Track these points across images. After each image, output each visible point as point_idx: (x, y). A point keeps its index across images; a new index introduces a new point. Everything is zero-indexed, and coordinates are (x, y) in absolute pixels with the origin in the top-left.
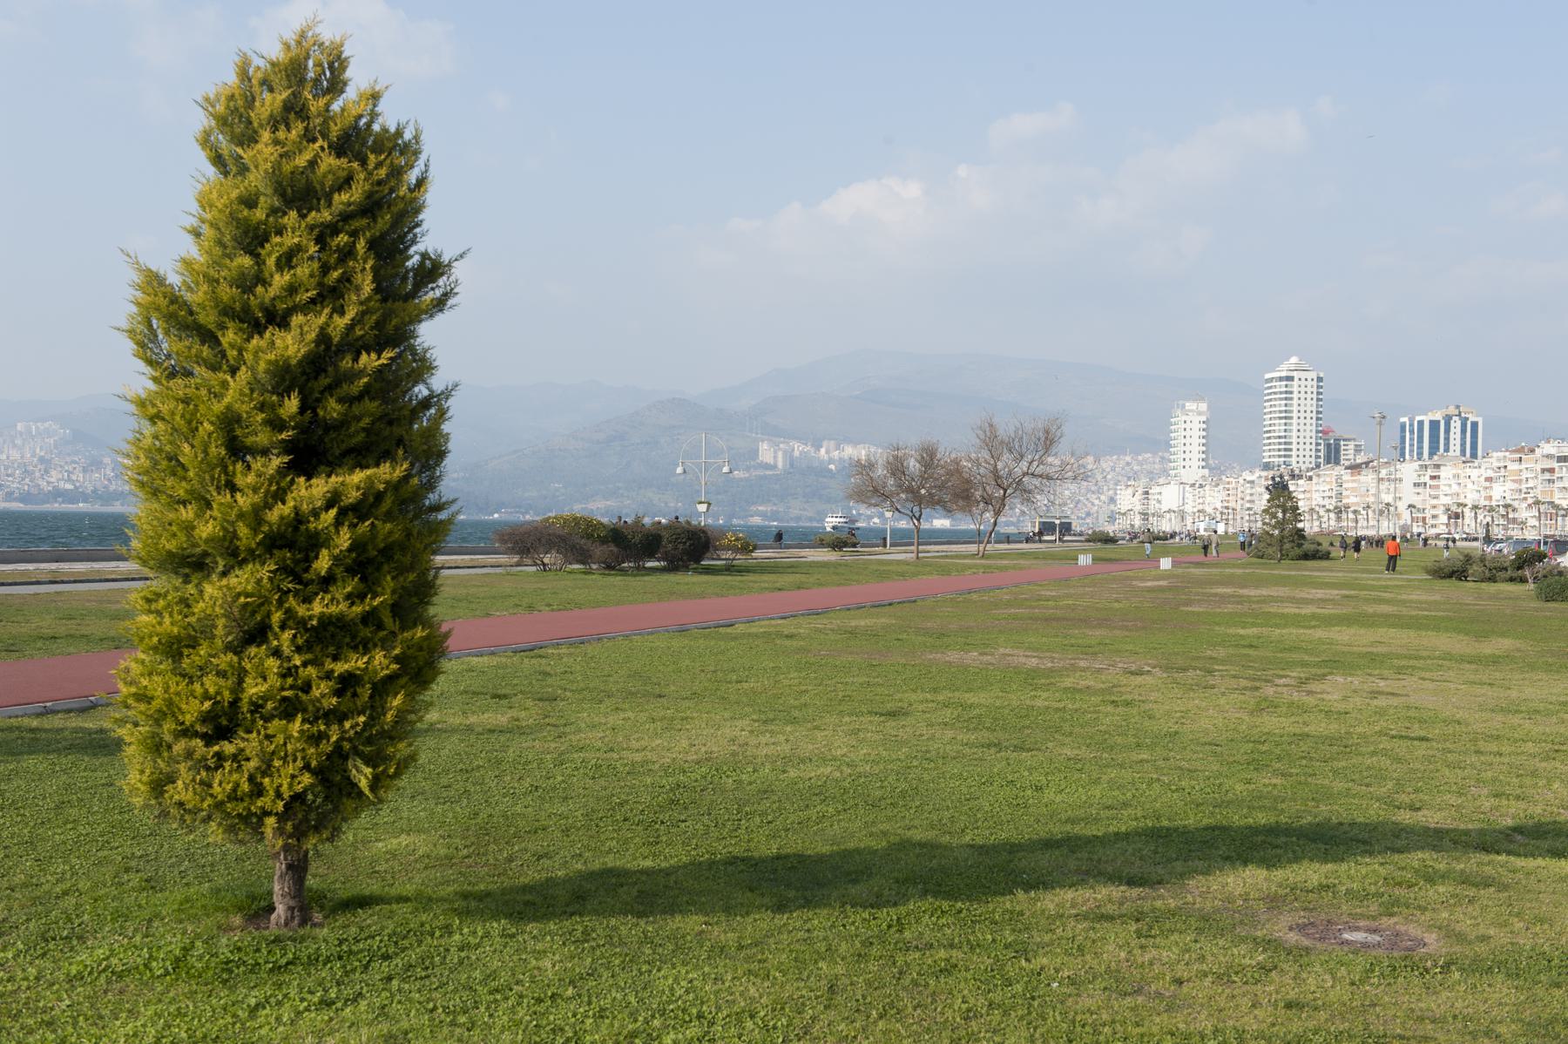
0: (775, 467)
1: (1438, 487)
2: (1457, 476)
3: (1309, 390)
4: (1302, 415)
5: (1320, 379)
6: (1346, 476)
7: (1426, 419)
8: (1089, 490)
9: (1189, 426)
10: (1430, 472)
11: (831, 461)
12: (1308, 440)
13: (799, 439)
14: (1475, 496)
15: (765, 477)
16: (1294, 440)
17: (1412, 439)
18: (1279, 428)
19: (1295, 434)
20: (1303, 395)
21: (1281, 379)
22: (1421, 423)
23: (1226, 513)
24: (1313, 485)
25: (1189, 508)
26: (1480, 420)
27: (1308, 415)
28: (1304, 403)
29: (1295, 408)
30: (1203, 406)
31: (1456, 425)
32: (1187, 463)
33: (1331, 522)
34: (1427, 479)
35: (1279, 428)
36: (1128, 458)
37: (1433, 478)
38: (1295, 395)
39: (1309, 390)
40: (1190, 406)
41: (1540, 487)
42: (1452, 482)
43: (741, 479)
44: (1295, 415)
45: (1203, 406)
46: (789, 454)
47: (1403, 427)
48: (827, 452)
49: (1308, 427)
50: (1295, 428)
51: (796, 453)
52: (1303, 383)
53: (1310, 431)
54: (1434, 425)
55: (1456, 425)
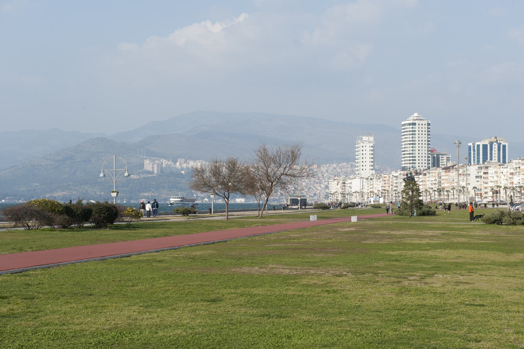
0: (152, 172)
1: (487, 178)
2: (496, 172)
3: (423, 130)
4: (420, 142)
5: (429, 124)
6: (443, 173)
7: (481, 144)
8: (315, 182)
9: (365, 148)
10: (483, 170)
11: (182, 169)
12: (424, 155)
13: (165, 158)
14: (506, 182)
15: (148, 178)
16: (417, 155)
17: (474, 154)
18: (409, 149)
19: (417, 152)
20: (420, 132)
21: (410, 124)
22: (478, 146)
23: (384, 193)
24: (427, 178)
25: (365, 191)
26: (507, 144)
28: (421, 137)
29: (417, 139)
30: (372, 139)
31: (495, 146)
32: (364, 168)
33: (436, 197)
34: (482, 174)
35: (409, 149)
36: (334, 166)
37: (485, 173)
38: (417, 133)
39: (423, 130)
40: (365, 138)
42: (494, 175)
43: (135, 179)
44: (417, 142)
45: (372, 139)
47: (470, 148)
48: (180, 164)
49: (423, 149)
50: (417, 149)
51: (164, 165)
52: (421, 126)
53: (424, 151)
54: (485, 147)
55: (495, 146)
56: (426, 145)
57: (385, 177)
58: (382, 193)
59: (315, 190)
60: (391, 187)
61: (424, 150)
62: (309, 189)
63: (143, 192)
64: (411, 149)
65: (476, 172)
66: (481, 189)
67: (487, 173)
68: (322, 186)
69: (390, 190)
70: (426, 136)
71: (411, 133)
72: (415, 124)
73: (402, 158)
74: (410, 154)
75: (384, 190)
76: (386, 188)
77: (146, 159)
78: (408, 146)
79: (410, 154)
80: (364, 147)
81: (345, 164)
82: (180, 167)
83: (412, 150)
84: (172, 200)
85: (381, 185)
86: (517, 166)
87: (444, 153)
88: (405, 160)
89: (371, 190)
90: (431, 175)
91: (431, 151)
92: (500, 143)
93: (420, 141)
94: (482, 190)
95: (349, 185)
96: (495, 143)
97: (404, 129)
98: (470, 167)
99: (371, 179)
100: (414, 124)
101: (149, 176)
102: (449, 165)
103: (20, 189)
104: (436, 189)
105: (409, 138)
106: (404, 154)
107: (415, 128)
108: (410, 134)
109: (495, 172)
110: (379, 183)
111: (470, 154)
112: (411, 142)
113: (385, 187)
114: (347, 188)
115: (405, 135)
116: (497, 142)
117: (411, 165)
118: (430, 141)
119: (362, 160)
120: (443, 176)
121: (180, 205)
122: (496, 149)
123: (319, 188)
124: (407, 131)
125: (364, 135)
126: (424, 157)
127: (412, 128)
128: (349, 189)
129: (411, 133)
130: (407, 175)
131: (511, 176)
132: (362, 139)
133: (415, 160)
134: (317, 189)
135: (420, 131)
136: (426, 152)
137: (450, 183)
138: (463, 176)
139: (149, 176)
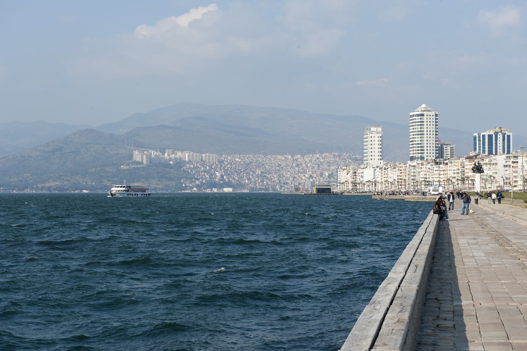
0: (142, 163)
3: (432, 120)
4: (429, 133)
5: (436, 115)
7: (486, 134)
8: (299, 172)
9: (373, 139)
11: (171, 159)
12: (432, 145)
13: (152, 148)
15: (137, 168)
16: (425, 145)
17: (479, 144)
18: (418, 139)
19: (425, 142)
20: (429, 123)
21: (418, 115)
22: (484, 136)
23: (401, 181)
24: (448, 167)
25: (378, 180)
26: (511, 134)
27: (432, 133)
28: (429, 128)
29: (425, 130)
30: (380, 129)
31: (500, 136)
32: (373, 158)
33: (372, 188)
34: (510, 163)
35: (418, 139)
36: (318, 156)
37: (514, 162)
38: (425, 123)
39: (432, 120)
40: (373, 129)
43: (125, 170)
44: (425, 133)
45: (380, 129)
46: (149, 157)
47: (475, 138)
48: (168, 155)
49: (432, 139)
51: (153, 156)
52: (429, 117)
53: (432, 141)
54: (490, 137)
55: (500, 136)
56: (434, 136)
57: (401, 167)
58: (398, 182)
59: (300, 179)
60: (407, 176)
62: (294, 178)
63: (133, 182)
64: (420, 139)
65: (504, 161)
66: (509, 178)
67: (517, 162)
68: (306, 175)
69: (407, 179)
70: (434, 126)
71: (420, 123)
72: (423, 115)
73: (410, 148)
74: (418, 144)
75: (401, 179)
76: (402, 178)
77: (135, 150)
78: (417, 136)
79: (418, 144)
81: (328, 154)
82: (168, 158)
83: (421, 141)
84: (114, 190)
85: (397, 174)
87: (447, 143)
89: (386, 179)
90: (453, 164)
92: (505, 134)
94: (511, 179)
95: (360, 175)
96: (499, 133)
97: (413, 120)
98: (497, 156)
99: (385, 169)
101: (139, 166)
103: (11, 180)
104: (460, 178)
105: (418, 128)
106: (413, 144)
107: (423, 119)
108: (418, 125)
110: (394, 173)
111: (475, 144)
112: (420, 133)
113: (401, 176)
114: (358, 177)
115: (413, 126)
116: (501, 132)
117: (420, 155)
118: (437, 132)
119: (371, 150)
121: (126, 195)
123: (304, 178)
124: (415, 122)
125: (372, 126)
127: (421, 119)
128: (361, 179)
129: (420, 123)
132: (370, 129)
134: (302, 179)
136: (434, 142)
138: (489, 166)
139: (139, 166)
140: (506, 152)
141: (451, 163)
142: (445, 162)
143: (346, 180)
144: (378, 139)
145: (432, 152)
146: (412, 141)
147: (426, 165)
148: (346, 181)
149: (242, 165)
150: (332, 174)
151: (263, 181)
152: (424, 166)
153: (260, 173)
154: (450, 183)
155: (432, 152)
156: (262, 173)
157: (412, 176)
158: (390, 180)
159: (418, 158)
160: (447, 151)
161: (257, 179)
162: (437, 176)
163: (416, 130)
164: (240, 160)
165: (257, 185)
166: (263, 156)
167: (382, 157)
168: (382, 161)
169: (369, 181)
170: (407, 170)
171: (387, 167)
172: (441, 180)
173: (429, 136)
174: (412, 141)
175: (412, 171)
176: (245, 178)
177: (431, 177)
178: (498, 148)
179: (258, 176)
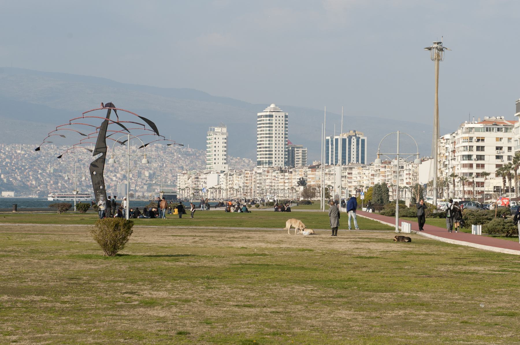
1: (351, 178)
2: (359, 173)
3: (281, 122)
4: (277, 135)
6: (309, 172)
9: (217, 140)
10: (348, 171)
14: (367, 182)
16: (274, 149)
17: (332, 148)
18: (266, 143)
19: (274, 146)
20: (278, 125)
21: (266, 116)
22: (337, 140)
25: (223, 186)
26: (365, 138)
27: (281, 136)
28: (278, 130)
29: (274, 132)
30: (225, 130)
31: (354, 140)
32: (217, 161)
34: (346, 174)
37: (349, 174)
38: (274, 125)
39: (281, 122)
40: (217, 129)
41: (393, 179)
42: (358, 176)
44: (274, 135)
45: (225, 130)
47: (327, 141)
49: (281, 142)
50: (274, 142)
52: (278, 118)
54: (344, 140)
55: (354, 140)
57: (247, 174)
60: (253, 183)
61: (281, 144)
64: (268, 142)
67: (352, 173)
68: (118, 175)
71: (268, 125)
73: (258, 151)
74: (266, 147)
78: (264, 139)
79: (266, 147)
80: (217, 138)
83: (269, 144)
85: (242, 181)
86: (378, 169)
88: (261, 155)
89: (231, 186)
91: (287, 143)
92: (359, 138)
93: (278, 134)
95: (203, 180)
96: (354, 137)
97: (261, 121)
98: (336, 167)
99: (230, 175)
100: (271, 116)
102: (314, 164)
105: (266, 130)
106: (260, 148)
107: (272, 120)
108: (266, 127)
109: (358, 173)
110: (239, 179)
112: (268, 135)
116: (355, 136)
117: (268, 159)
118: (287, 134)
120: (310, 174)
122: (355, 144)
123: (114, 178)
124: (263, 124)
125: (216, 126)
126: (281, 151)
127: (269, 120)
128: (204, 185)
129: (268, 125)
130: (300, 179)
131: (372, 177)
132: (214, 129)
133: (272, 154)
134: (112, 180)
135: (278, 123)
136: (283, 146)
137: (317, 181)
138: (328, 176)
140: (340, 162)
141: (295, 171)
142: (290, 170)
143: (186, 186)
144: (222, 149)
145: (281, 156)
146: (260, 144)
147: (272, 173)
148: (187, 187)
149: (26, 159)
150: (154, 173)
151: (57, 183)
152: (270, 174)
153: (52, 171)
154: (294, 191)
155: (281, 156)
156: (55, 170)
157: (258, 183)
158: (236, 187)
159: (266, 163)
160: (299, 154)
161: (48, 179)
162: (282, 184)
163: (265, 132)
164: (23, 152)
165: (49, 187)
166: (55, 147)
167: (227, 162)
168: (226, 166)
169: (213, 188)
170: (253, 177)
171: (232, 173)
172: (286, 188)
173: (277, 139)
174: (260, 144)
175: (258, 178)
176: (31, 178)
177: (276, 185)
178: (352, 156)
179: (49, 175)
